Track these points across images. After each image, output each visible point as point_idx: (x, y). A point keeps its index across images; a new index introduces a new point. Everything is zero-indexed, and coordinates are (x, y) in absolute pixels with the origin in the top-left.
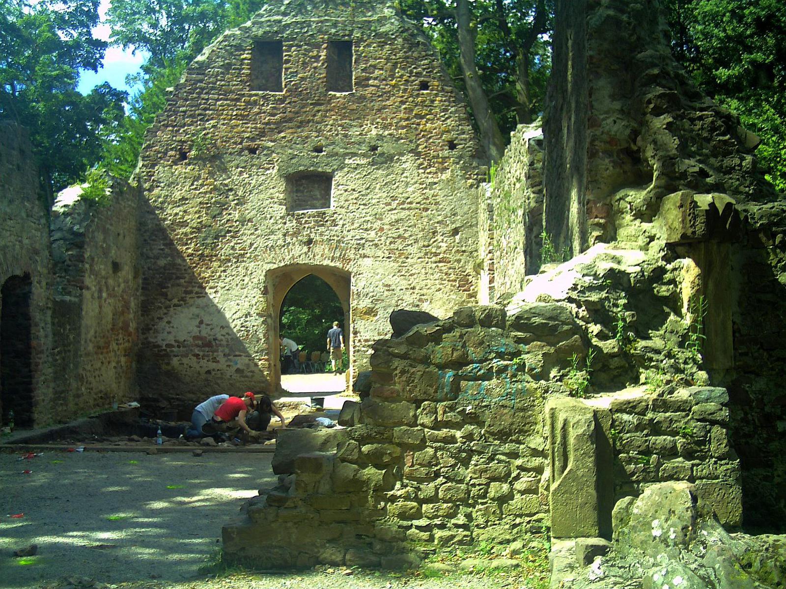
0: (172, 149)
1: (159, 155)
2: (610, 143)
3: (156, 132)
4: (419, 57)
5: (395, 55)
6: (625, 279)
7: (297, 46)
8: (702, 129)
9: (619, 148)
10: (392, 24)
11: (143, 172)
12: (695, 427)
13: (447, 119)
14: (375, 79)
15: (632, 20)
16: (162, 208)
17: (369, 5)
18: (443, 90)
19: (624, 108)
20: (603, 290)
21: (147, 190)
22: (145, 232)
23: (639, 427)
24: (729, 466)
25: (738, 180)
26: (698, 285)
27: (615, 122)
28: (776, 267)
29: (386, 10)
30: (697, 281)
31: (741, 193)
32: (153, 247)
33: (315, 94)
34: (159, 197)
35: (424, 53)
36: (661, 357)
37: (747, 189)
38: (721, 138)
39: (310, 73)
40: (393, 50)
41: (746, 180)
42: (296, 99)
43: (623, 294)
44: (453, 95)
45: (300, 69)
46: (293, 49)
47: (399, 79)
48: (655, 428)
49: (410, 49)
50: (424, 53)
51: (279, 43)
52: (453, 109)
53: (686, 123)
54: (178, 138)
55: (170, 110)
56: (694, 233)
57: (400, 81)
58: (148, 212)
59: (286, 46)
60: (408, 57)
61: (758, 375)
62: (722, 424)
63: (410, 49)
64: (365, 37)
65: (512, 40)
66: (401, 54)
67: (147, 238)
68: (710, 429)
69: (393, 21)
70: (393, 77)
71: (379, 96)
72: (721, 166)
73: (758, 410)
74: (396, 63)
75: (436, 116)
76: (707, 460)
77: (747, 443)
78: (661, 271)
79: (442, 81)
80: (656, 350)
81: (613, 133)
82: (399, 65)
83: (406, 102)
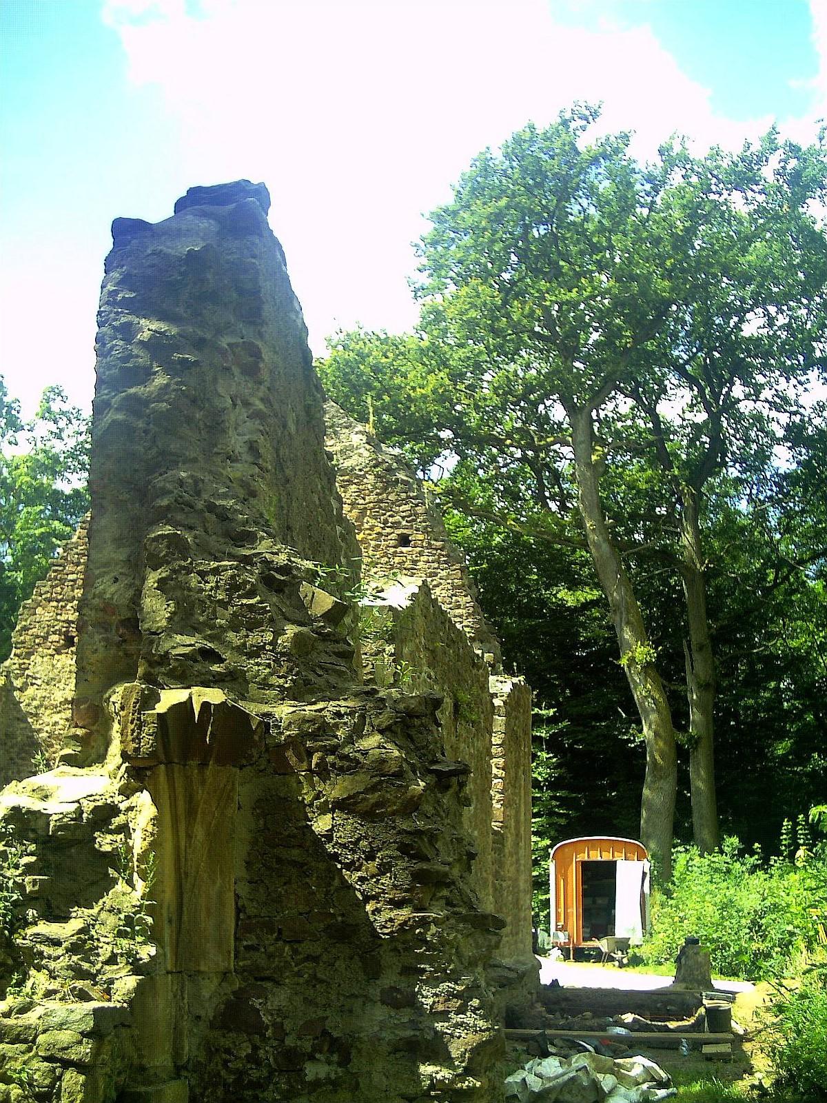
0: (54, 633)
1: (37, 641)
3: (35, 609)
5: (364, 499)
6: (41, 822)
8: (217, 587)
9: (119, 618)
10: (360, 455)
11: (15, 664)
12: (39, 1070)
15: (151, 426)
16: (36, 715)
18: (430, 546)
19: (131, 559)
21: (19, 689)
22: (12, 747)
26: (152, 834)
27: (116, 580)
28: (311, 805)
29: (352, 436)
30: (150, 828)
31: (271, 686)
32: (21, 768)
34: (33, 699)
35: (403, 495)
36: (60, 951)
37: (281, 681)
38: (244, 601)
41: (281, 666)
43: (32, 847)
49: (385, 489)
50: (403, 495)
53: (194, 580)
54: (64, 617)
55: (55, 578)
56: (137, 750)
58: (18, 719)
60: (381, 501)
61: (278, 983)
62: (79, 1066)
63: (385, 489)
66: (372, 497)
67: (14, 755)
68: (62, 1075)
69: (360, 451)
72: (244, 645)
73: (275, 1043)
77: (256, 1097)
78: (113, 810)
79: (428, 533)
80: (52, 940)
81: (108, 596)
82: (368, 512)
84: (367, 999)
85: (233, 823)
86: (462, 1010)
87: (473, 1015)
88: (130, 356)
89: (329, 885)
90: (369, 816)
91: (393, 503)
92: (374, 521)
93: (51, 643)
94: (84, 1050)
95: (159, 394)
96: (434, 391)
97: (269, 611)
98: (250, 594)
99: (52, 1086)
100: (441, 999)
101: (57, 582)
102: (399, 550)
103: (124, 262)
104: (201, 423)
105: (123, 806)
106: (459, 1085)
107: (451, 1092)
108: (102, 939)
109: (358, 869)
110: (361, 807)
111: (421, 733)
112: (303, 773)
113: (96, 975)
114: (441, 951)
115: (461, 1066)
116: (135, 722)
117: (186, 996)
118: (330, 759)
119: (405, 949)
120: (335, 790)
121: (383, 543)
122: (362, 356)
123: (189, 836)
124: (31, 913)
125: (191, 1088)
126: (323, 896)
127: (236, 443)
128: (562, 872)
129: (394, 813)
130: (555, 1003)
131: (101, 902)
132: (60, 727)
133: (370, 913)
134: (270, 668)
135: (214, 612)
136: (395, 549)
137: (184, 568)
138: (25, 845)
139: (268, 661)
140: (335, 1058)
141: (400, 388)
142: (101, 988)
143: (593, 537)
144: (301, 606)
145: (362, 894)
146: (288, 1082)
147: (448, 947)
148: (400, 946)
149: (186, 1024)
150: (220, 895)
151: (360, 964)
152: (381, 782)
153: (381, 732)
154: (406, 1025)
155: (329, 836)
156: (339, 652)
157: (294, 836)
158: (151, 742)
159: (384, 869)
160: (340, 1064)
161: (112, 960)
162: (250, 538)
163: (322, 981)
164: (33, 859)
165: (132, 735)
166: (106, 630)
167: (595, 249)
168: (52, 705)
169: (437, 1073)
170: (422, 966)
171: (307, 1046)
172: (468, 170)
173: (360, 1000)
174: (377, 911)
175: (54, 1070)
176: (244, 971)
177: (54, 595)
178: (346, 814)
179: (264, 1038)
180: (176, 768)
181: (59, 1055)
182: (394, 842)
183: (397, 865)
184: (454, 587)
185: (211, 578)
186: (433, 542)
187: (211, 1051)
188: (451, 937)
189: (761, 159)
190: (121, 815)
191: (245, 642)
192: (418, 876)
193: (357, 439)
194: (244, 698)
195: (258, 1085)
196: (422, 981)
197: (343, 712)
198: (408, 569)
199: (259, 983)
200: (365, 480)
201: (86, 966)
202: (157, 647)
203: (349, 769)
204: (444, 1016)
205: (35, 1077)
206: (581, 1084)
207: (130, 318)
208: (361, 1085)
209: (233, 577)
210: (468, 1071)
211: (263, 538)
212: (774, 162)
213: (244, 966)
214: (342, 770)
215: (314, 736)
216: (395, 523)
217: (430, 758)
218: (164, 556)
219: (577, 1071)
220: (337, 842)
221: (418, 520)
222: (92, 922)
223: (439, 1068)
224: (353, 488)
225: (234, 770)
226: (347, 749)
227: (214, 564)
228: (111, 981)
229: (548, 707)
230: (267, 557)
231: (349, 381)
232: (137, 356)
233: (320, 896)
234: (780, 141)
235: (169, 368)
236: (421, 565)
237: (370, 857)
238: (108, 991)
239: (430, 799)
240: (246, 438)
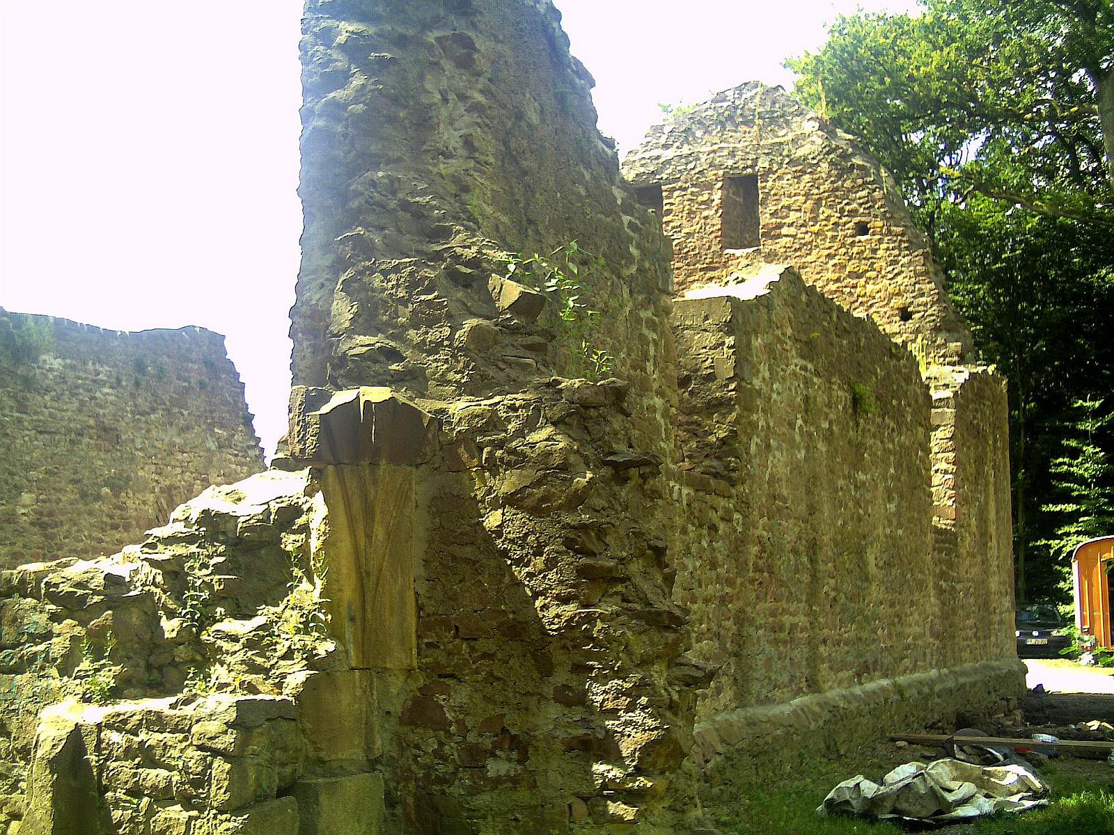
2: (311, 317)
4: (853, 187)
6: (230, 525)
7: (681, 188)
8: (398, 285)
10: (813, 143)
13: (897, 275)
14: (790, 225)
17: (782, 120)
18: (889, 232)
20: (192, 543)
23: (129, 753)
24: (231, 825)
25: (446, 361)
28: (482, 501)
29: (805, 124)
30: (323, 528)
33: (706, 254)
36: (238, 646)
37: (459, 376)
38: (423, 297)
39: (699, 226)
40: (814, 180)
42: (680, 265)
43: (222, 548)
44: (905, 239)
45: (684, 222)
46: (676, 194)
47: (824, 223)
48: (148, 757)
49: (839, 177)
50: (860, 181)
51: (657, 188)
52: (906, 260)
53: (377, 280)
57: (826, 225)
59: (666, 191)
60: (837, 189)
63: (839, 177)
64: (775, 167)
65: (875, 149)
66: (827, 186)
68: (212, 763)
70: (815, 220)
71: (796, 250)
73: (459, 739)
74: (820, 199)
75: (880, 272)
76: (206, 812)
77: (443, 793)
79: (888, 219)
82: (824, 202)
83: (835, 255)
84: (542, 697)
85: (411, 523)
86: (630, 708)
87: (642, 714)
88: (331, 61)
89: (500, 582)
90: (536, 511)
91: (849, 191)
92: (830, 211)
94: (227, 741)
96: (940, 68)
98: (428, 291)
99: (203, 772)
100: (610, 696)
104: (406, 121)
106: (630, 785)
107: (624, 793)
108: (283, 636)
109: (527, 565)
110: (529, 502)
111: (599, 424)
112: (474, 469)
113: (270, 670)
114: (607, 648)
115: (631, 765)
117: (375, 693)
118: (499, 453)
119: (574, 647)
120: (506, 484)
121: (840, 233)
122: (859, 40)
123: (369, 536)
124: (220, 610)
125: (386, 782)
126: (495, 593)
127: (450, 137)
128: (1085, 574)
129: (560, 507)
130: (1037, 710)
133: (538, 609)
135: (396, 311)
136: (853, 239)
137: (368, 268)
139: (445, 357)
140: (514, 755)
141: (902, 68)
142: (272, 682)
144: (490, 300)
145: (531, 590)
146: (472, 778)
147: (615, 644)
148: (569, 644)
149: (376, 719)
150: (402, 594)
151: (533, 661)
152: (546, 476)
153: (554, 424)
154: (579, 723)
155: (499, 532)
156: (528, 345)
157: (466, 534)
158: (314, 443)
159: (551, 564)
160: (520, 762)
161: (288, 655)
162: (446, 233)
163: (498, 679)
164: (221, 559)
165: (298, 436)
166: (316, 337)
169: (609, 771)
170: (591, 663)
171: (487, 743)
173: (535, 698)
174: (545, 607)
176: (427, 668)
178: (516, 509)
179: (449, 735)
180: (347, 469)
181: (209, 744)
182: (558, 537)
183: (562, 560)
185: (393, 276)
186: (893, 228)
187: (403, 747)
188: (618, 633)
190: (304, 516)
192: (582, 572)
193: (809, 127)
194: (423, 396)
195: (442, 781)
196: (591, 678)
197: (517, 405)
199: (442, 680)
201: (259, 660)
202: (336, 350)
203: (516, 463)
204: (613, 713)
205: (190, 764)
206: (917, 792)
207: (330, 23)
208: (539, 784)
209: (411, 274)
210: (639, 771)
211: (458, 232)
213: (426, 663)
214: (509, 465)
215: (483, 431)
217: (606, 450)
219: (914, 778)
220: (506, 538)
221: (876, 206)
222: (276, 619)
223: (610, 767)
224: (807, 178)
225: (409, 469)
226: (514, 443)
228: (283, 676)
229: (1093, 399)
230: (457, 251)
231: (846, 67)
232: (337, 61)
233: (492, 594)
235: (366, 68)
236: (880, 253)
237: (539, 553)
238: (279, 685)
239: (602, 491)
240: (462, 132)
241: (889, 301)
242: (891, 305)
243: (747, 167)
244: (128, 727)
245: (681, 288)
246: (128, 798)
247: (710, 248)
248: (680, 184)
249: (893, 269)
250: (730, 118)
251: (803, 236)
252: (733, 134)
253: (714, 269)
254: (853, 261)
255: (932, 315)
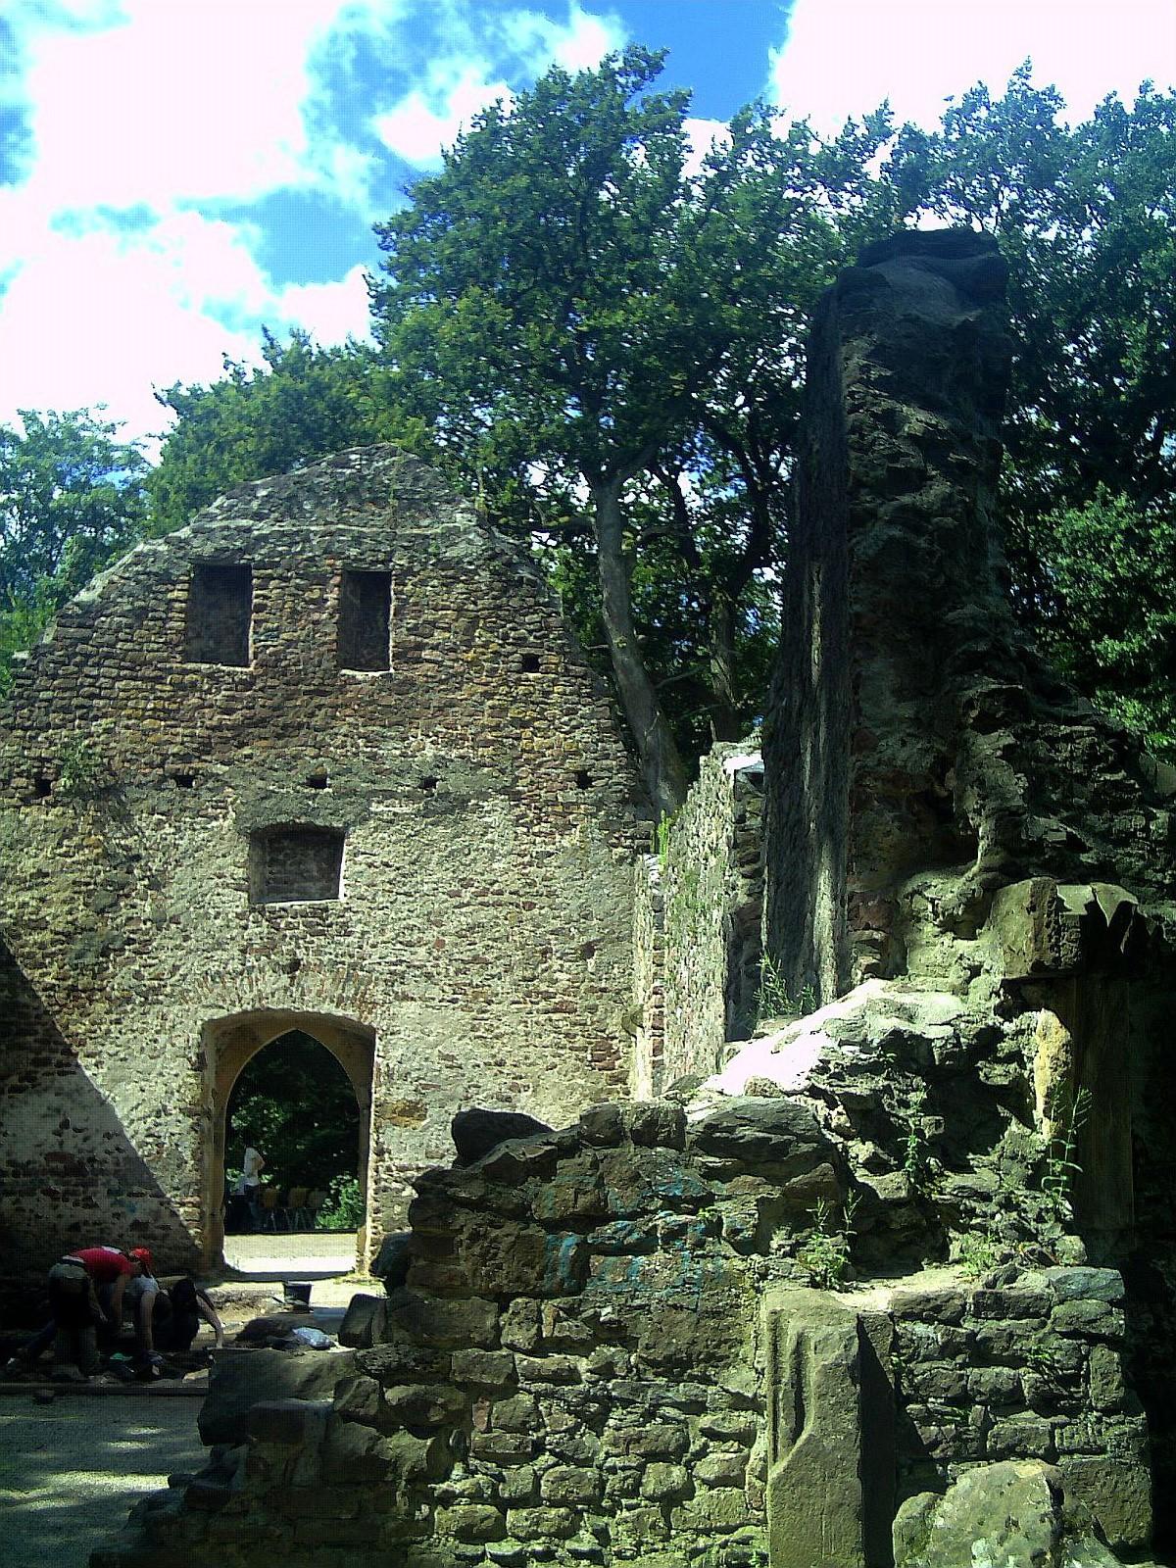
0: (20, 775)
5: (475, 603)
6: (923, 1049)
7: (281, 578)
10: (470, 542)
12: (1058, 1350)
15: (936, 547)
23: (948, 1350)
26: (1066, 1064)
36: (992, 1208)
37: (1159, 876)
39: (305, 632)
48: (980, 1352)
49: (504, 591)
55: (21, 696)
56: (1057, 960)
59: (258, 578)
60: (499, 608)
62: (1112, 1342)
63: (504, 591)
66: (487, 601)
68: (1088, 1353)
69: (471, 537)
71: (441, 682)
79: (565, 654)
91: (516, 611)
93: (16, 788)
95: (942, 505)
97: (1137, 790)
99: (1079, 1367)
101: (23, 701)
102: (523, 676)
103: (871, 329)
105: (1008, 1027)
116: (1052, 925)
131: (998, 1147)
132: (30, 910)
134: (1144, 860)
135: (1071, 787)
138: (908, 1077)
143: (621, 658)
167: (626, 253)
168: (19, 878)
172: (467, 130)
175: (1078, 1349)
177: (19, 720)
184: (601, 731)
189: (867, 148)
191: (1110, 827)
198: (538, 704)
199: (1159, 1241)
200: (477, 578)
209: (1092, 746)
212: (884, 153)
216: (519, 639)
218: (1003, 716)
227: (1065, 729)
232: (908, 455)
234: (896, 123)
241: (564, 761)
242: (567, 766)
243: (378, 562)
244: (946, 1314)
245: (275, 714)
246: (949, 1409)
247: (320, 662)
248: (280, 571)
249: (570, 720)
250: (354, 490)
251: (450, 663)
252: (357, 513)
253: (324, 694)
254: (518, 705)
255: (619, 784)
